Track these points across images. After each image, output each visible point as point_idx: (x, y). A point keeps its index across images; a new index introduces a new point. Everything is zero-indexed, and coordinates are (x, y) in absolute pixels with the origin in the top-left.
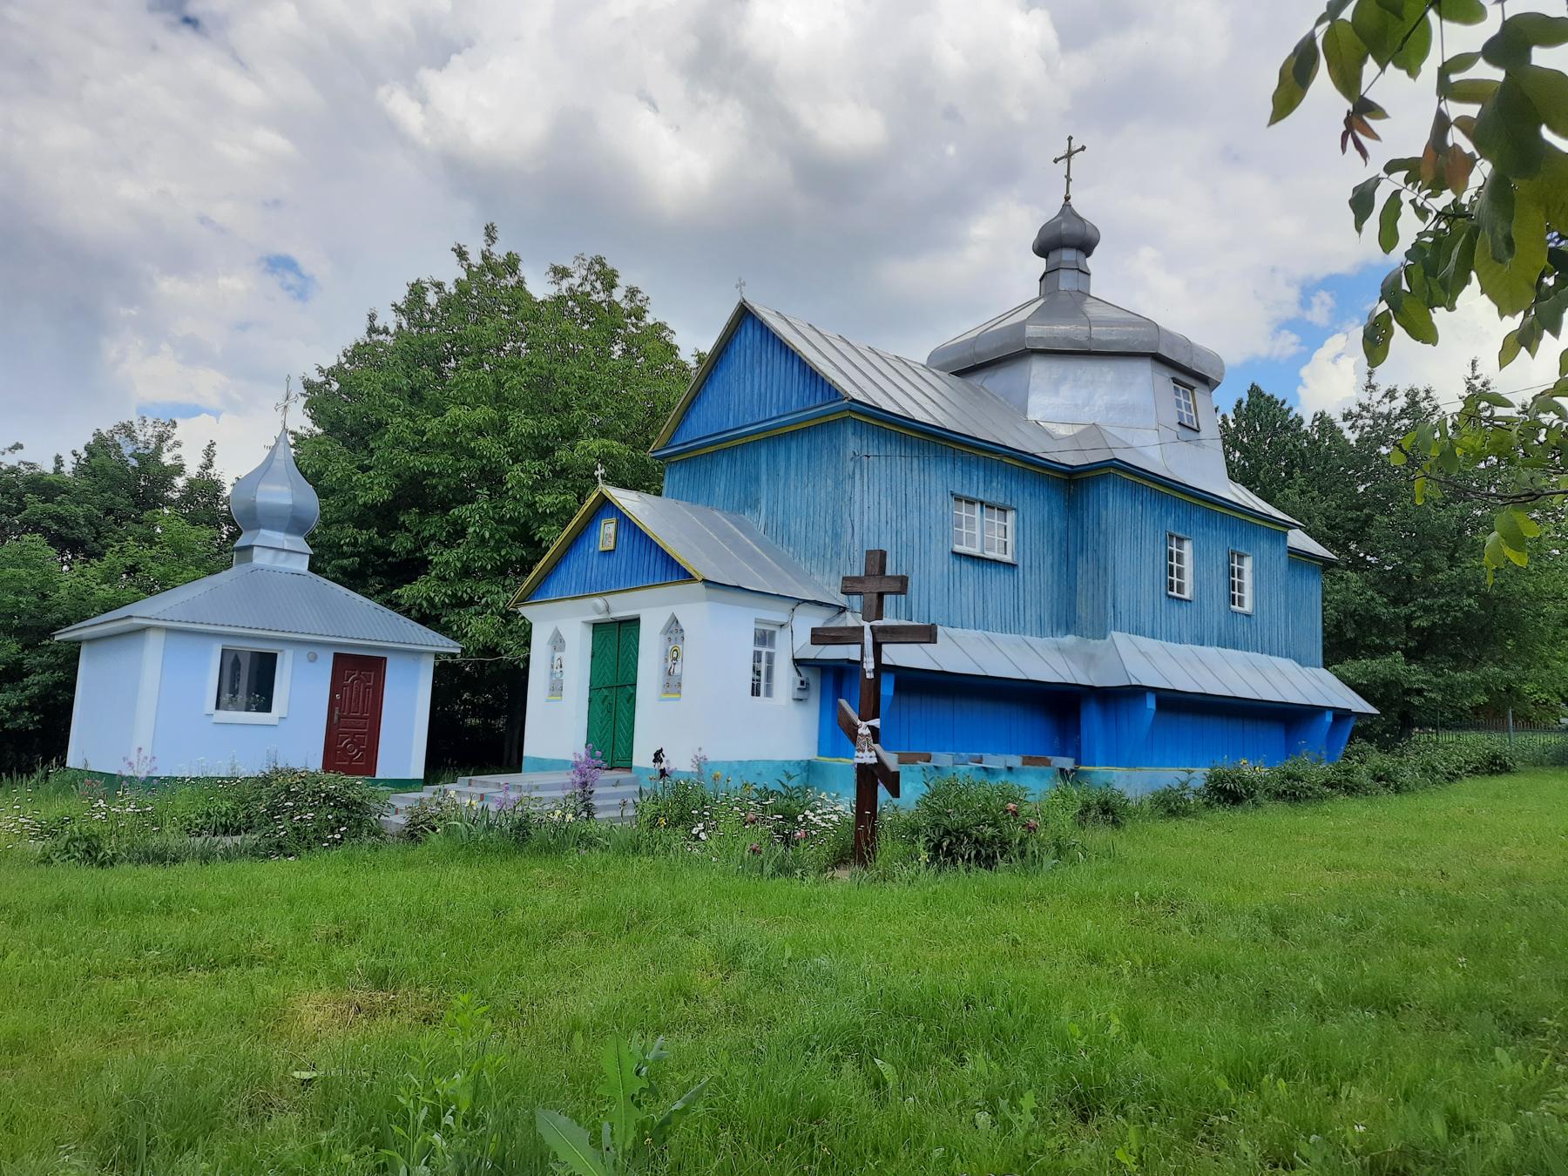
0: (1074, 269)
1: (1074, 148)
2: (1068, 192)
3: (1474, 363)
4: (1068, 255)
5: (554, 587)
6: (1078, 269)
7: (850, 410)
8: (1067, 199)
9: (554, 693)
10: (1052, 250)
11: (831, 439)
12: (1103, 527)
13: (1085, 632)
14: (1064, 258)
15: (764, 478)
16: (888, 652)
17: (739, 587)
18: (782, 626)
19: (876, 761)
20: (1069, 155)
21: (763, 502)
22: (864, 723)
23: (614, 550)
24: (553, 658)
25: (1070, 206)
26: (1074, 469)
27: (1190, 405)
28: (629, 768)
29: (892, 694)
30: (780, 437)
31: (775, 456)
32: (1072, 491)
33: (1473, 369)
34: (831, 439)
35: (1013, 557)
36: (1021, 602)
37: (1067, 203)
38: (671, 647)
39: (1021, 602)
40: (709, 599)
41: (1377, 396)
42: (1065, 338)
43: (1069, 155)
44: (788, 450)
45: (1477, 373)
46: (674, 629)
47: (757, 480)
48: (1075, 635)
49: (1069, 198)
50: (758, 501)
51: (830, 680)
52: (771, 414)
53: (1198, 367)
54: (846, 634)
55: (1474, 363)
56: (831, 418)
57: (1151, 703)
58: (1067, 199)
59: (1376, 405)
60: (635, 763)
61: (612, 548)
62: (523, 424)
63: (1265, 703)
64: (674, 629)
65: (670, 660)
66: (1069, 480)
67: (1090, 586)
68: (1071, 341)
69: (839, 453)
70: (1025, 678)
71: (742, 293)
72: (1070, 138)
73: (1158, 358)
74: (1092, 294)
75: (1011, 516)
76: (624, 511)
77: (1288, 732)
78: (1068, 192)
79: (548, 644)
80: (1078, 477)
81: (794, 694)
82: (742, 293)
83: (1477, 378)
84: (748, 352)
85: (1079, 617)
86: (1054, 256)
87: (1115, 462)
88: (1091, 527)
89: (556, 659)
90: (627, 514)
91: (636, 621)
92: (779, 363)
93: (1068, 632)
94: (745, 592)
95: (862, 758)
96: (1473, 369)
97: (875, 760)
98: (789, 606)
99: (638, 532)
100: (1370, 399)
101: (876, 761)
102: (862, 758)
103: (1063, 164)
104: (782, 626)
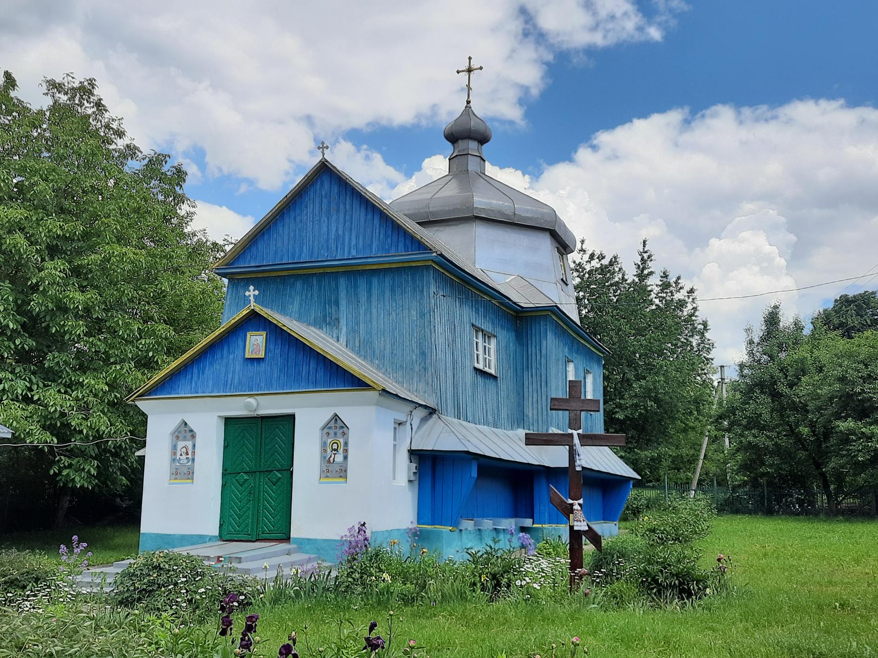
0: (477, 156)
3: (644, 242)
7: (432, 261)
8: (468, 102)
9: (177, 477)
10: (461, 139)
11: (414, 280)
12: (544, 352)
14: (470, 147)
17: (397, 396)
18: (400, 424)
20: (470, 70)
22: (576, 502)
24: (175, 447)
29: (476, 476)
30: (362, 273)
32: (518, 325)
33: (644, 246)
35: (495, 372)
37: (468, 105)
38: (329, 440)
40: (377, 404)
43: (470, 70)
44: (370, 284)
46: (336, 425)
47: (337, 304)
49: (470, 102)
50: (338, 320)
52: (349, 252)
53: (567, 241)
54: (556, 438)
55: (644, 242)
56: (414, 264)
57: (631, 482)
58: (468, 102)
60: (293, 535)
62: (55, 225)
63: (618, 477)
64: (336, 425)
65: (329, 450)
68: (501, 213)
70: (527, 462)
74: (486, 174)
75: (493, 341)
76: (285, 328)
77: (604, 495)
79: (170, 434)
80: (521, 315)
81: (409, 476)
82: (323, 154)
83: (646, 252)
85: (527, 416)
86: (462, 144)
87: (555, 308)
88: (534, 351)
89: (179, 448)
91: (292, 417)
92: (360, 215)
94: (388, 395)
95: (581, 526)
96: (644, 246)
97: (586, 528)
98: (408, 408)
99: (305, 346)
100: (582, 259)
102: (581, 526)
103: (465, 76)
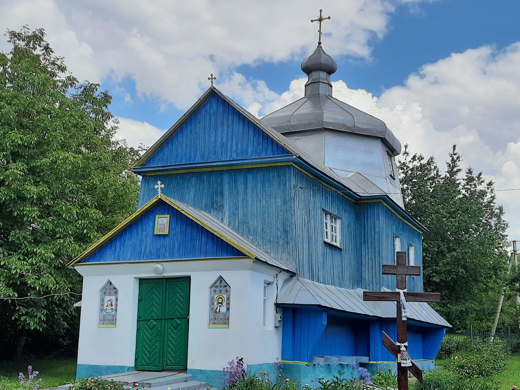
1: (323, 17)
2: (320, 40)
3: (454, 146)
4: (323, 75)
5: (109, 253)
6: (328, 84)
7: (293, 162)
8: (320, 43)
12: (377, 230)
13: (367, 287)
15: (226, 193)
16: (394, 305)
17: (266, 263)
18: (268, 284)
19: (412, 365)
21: (226, 207)
23: (168, 235)
25: (321, 47)
26: (362, 198)
27: (170, 139)
28: (185, 370)
29: (326, 324)
31: (236, 181)
33: (454, 150)
34: (279, 177)
35: (340, 245)
36: (344, 269)
38: (216, 296)
39: (344, 269)
41: (409, 158)
42: (342, 125)
44: (246, 179)
45: (455, 152)
47: (222, 194)
48: (362, 288)
50: (222, 206)
51: (290, 315)
52: (231, 156)
55: (454, 146)
58: (320, 43)
59: (408, 163)
61: (168, 234)
65: (216, 304)
66: (355, 204)
67: (370, 262)
69: (285, 184)
71: (212, 83)
72: (321, 11)
73: (384, 141)
74: (333, 96)
75: (339, 222)
76: (183, 212)
77: (424, 339)
78: (320, 40)
82: (212, 83)
83: (455, 154)
84: (213, 117)
87: (385, 196)
88: (369, 230)
89: (106, 301)
90: (186, 214)
91: (188, 278)
92: (239, 128)
93: (358, 287)
95: (406, 363)
96: (454, 150)
98: (274, 272)
101: (412, 365)
102: (406, 363)
104: (268, 284)
